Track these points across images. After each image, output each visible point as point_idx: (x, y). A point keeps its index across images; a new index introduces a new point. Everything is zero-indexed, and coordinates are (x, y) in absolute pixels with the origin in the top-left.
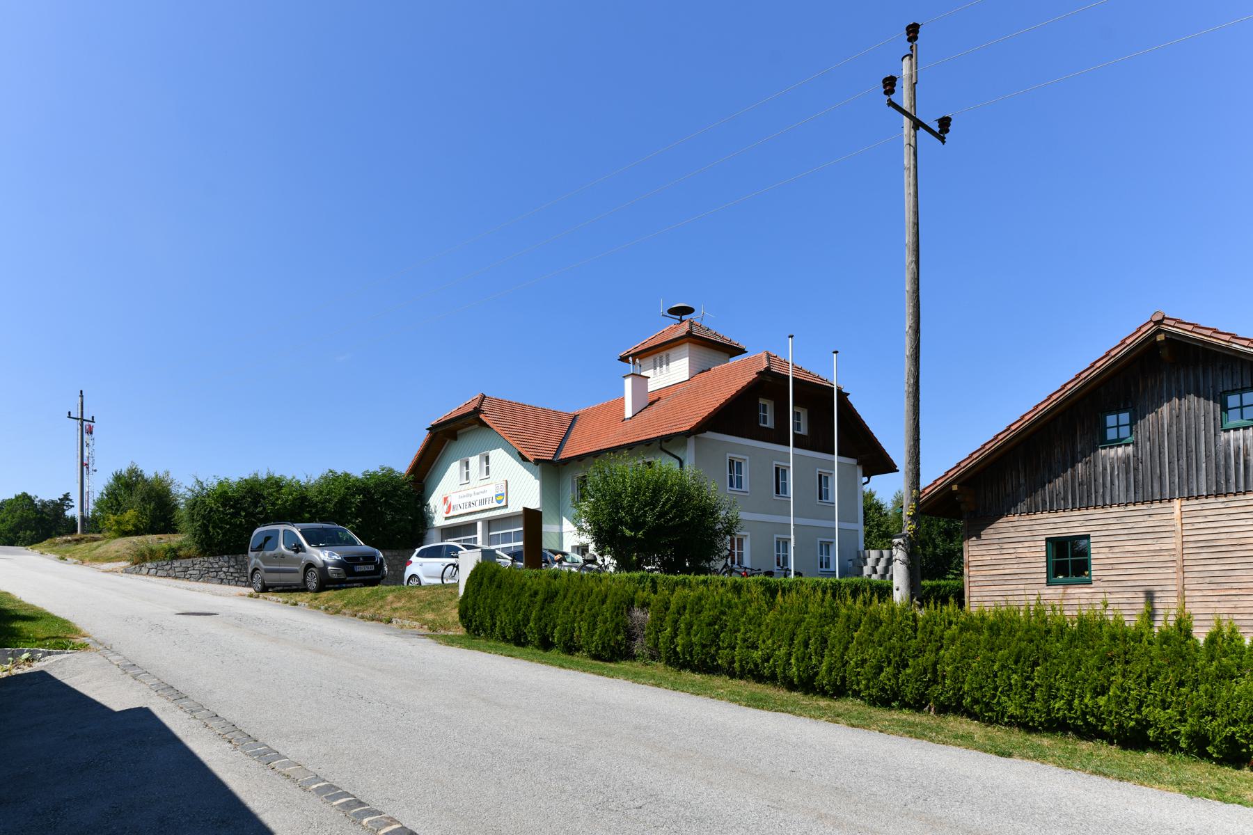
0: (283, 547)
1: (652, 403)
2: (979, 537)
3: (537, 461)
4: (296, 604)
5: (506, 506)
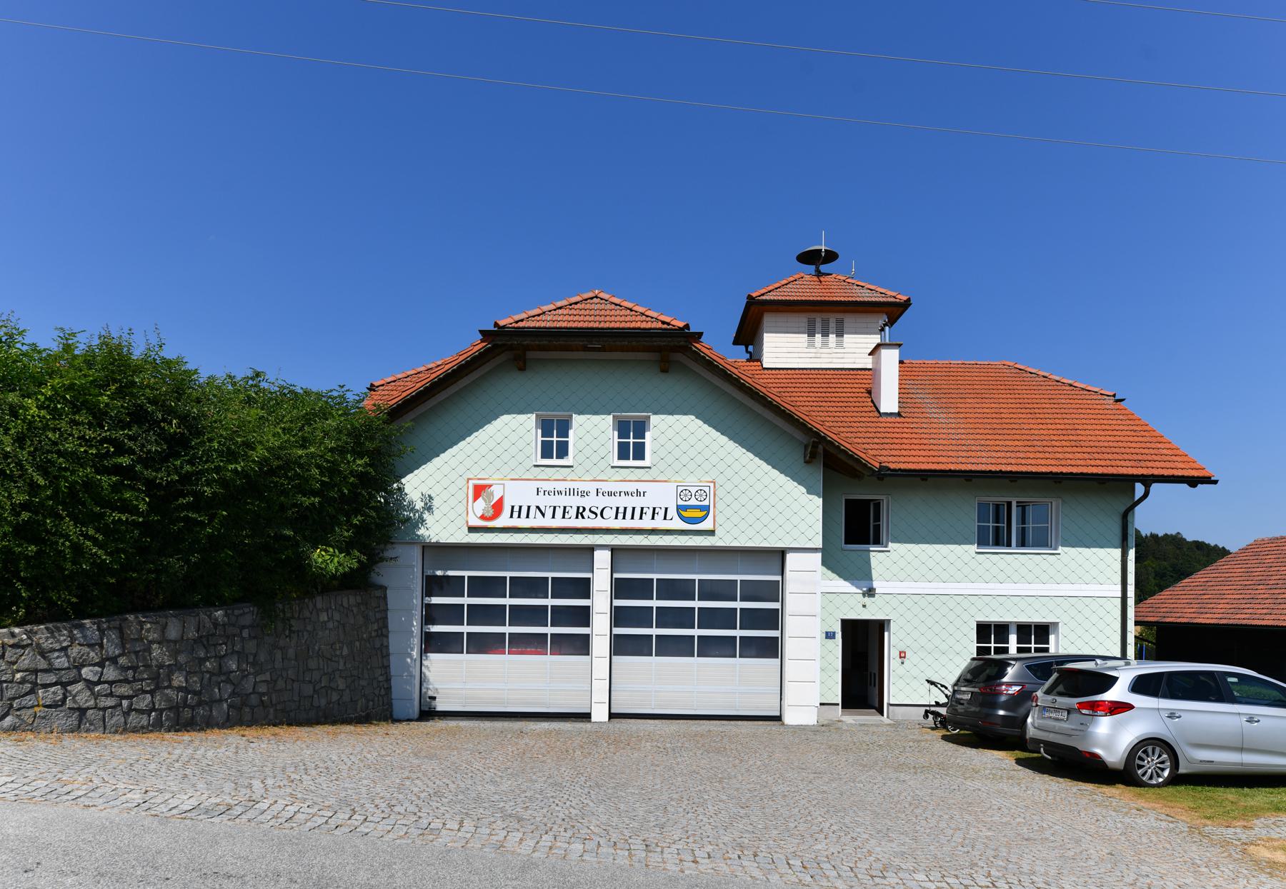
5: (712, 533)
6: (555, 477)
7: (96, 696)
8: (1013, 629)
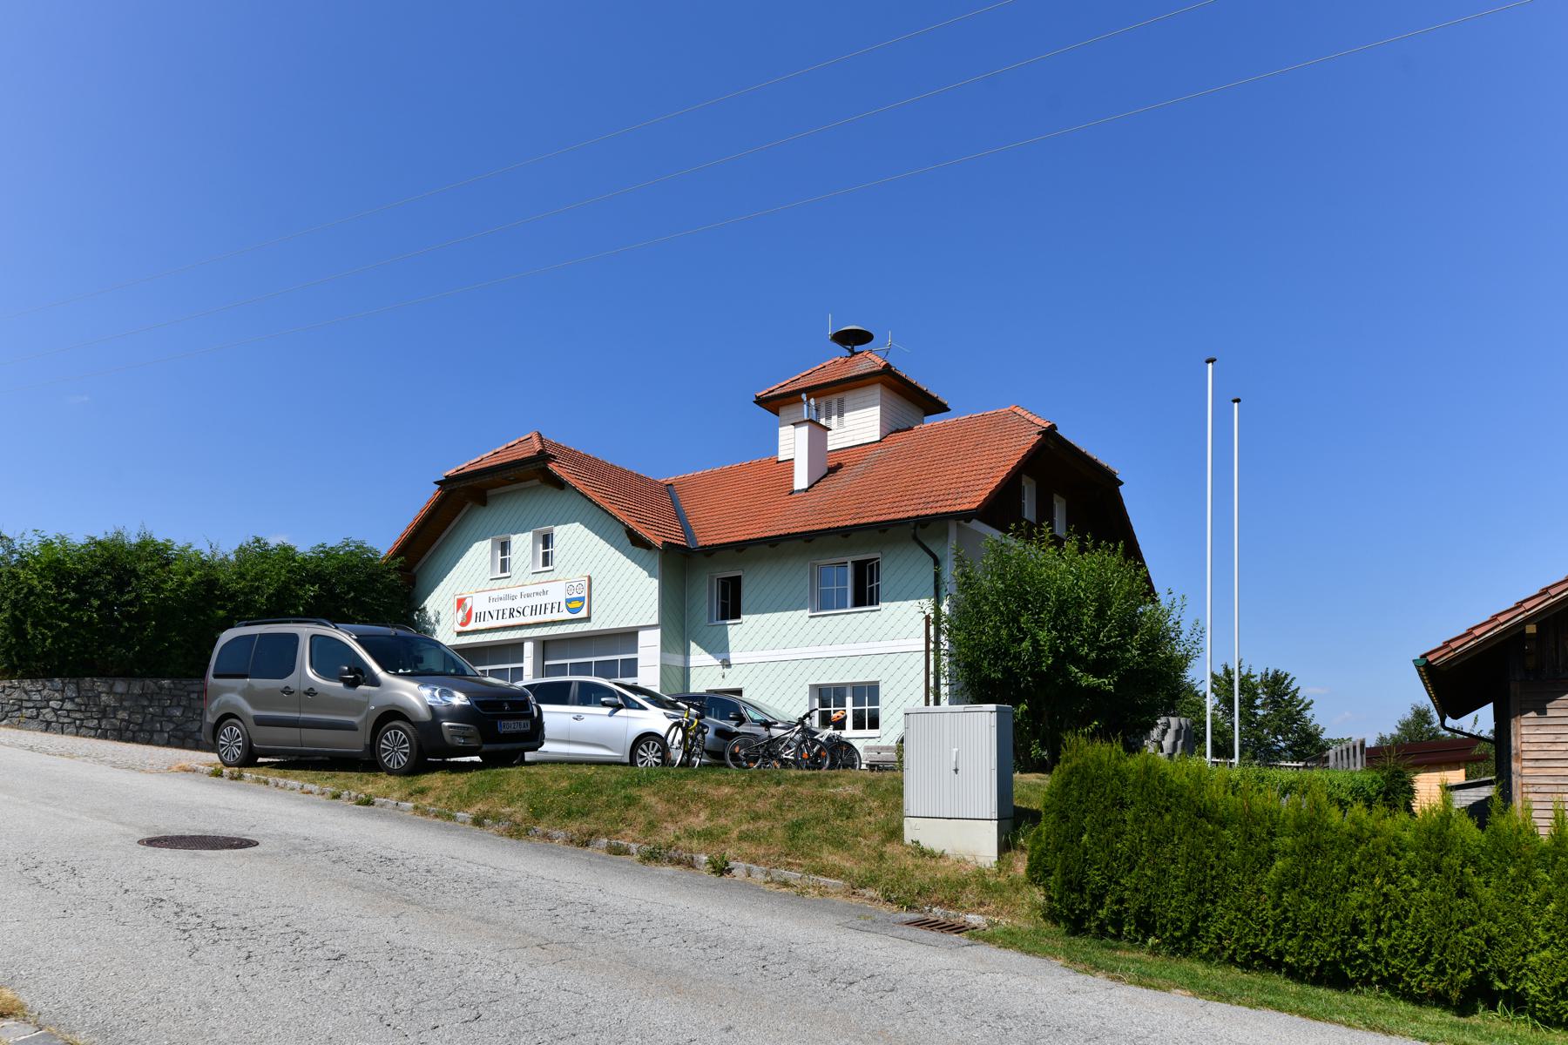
0: (310, 673)
1: (832, 470)
2: (1542, 711)
3: (669, 548)
4: (368, 802)
5: (588, 619)
6: (508, 587)
7: (58, 716)
8: (849, 691)
